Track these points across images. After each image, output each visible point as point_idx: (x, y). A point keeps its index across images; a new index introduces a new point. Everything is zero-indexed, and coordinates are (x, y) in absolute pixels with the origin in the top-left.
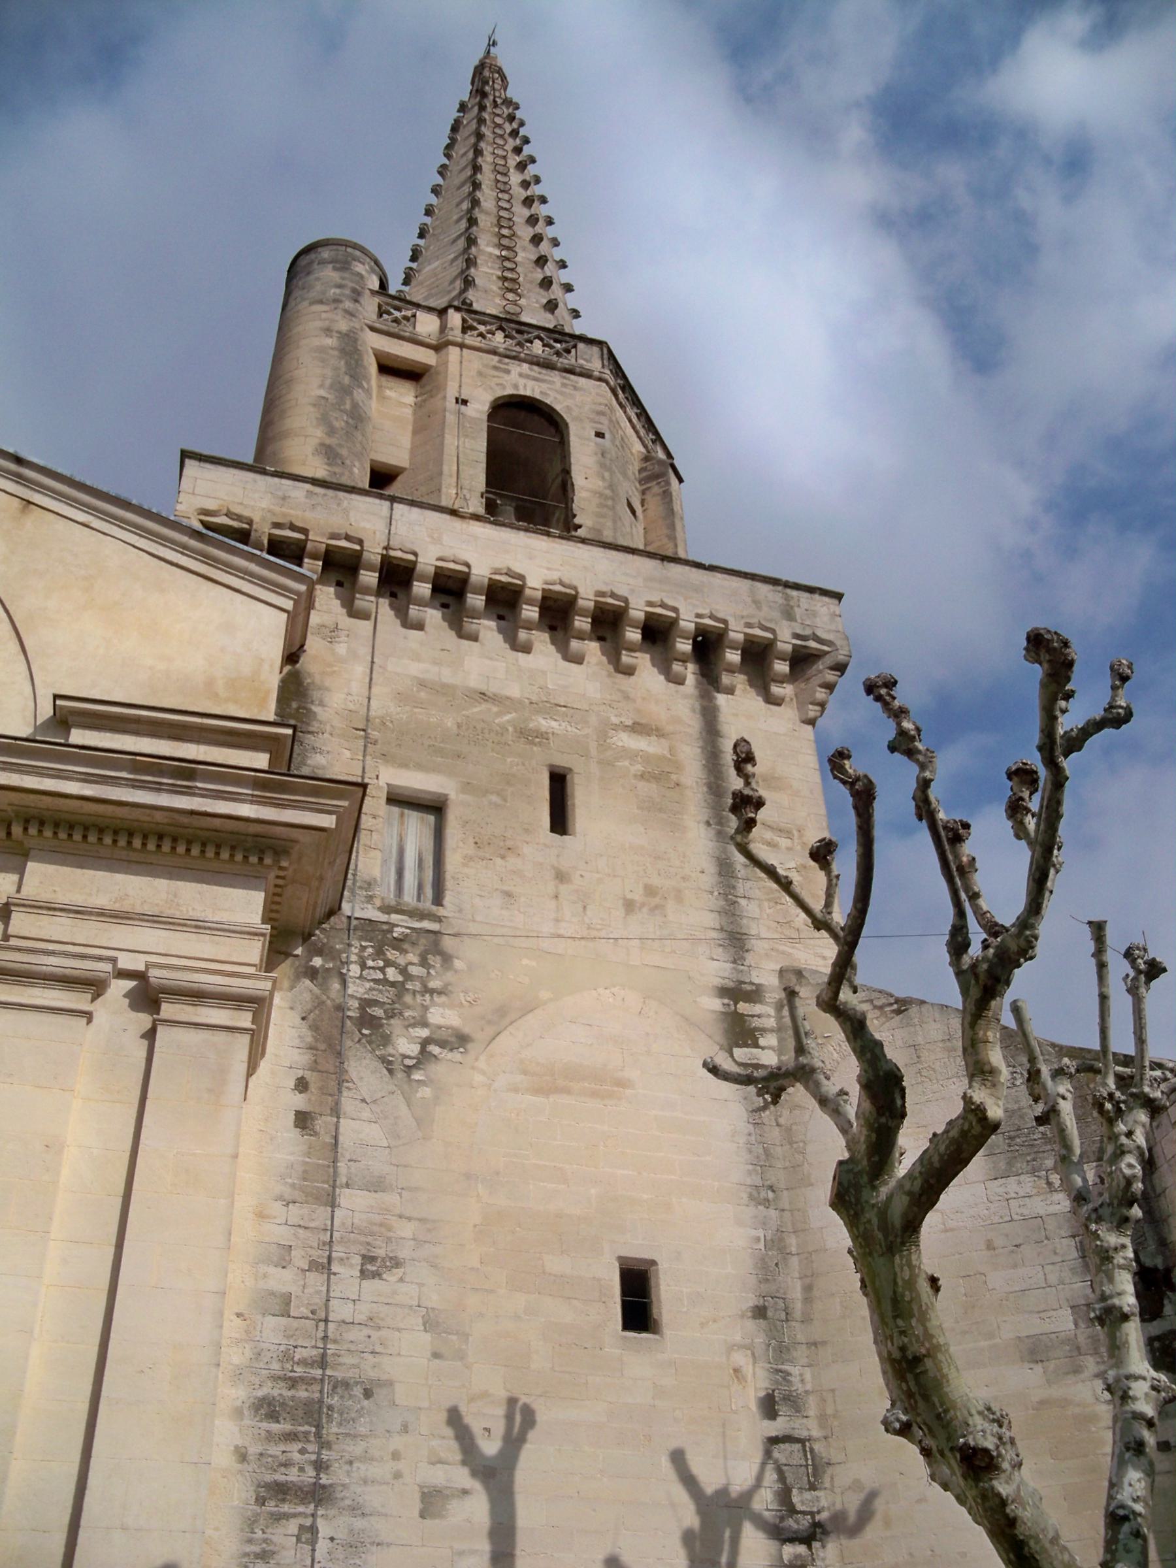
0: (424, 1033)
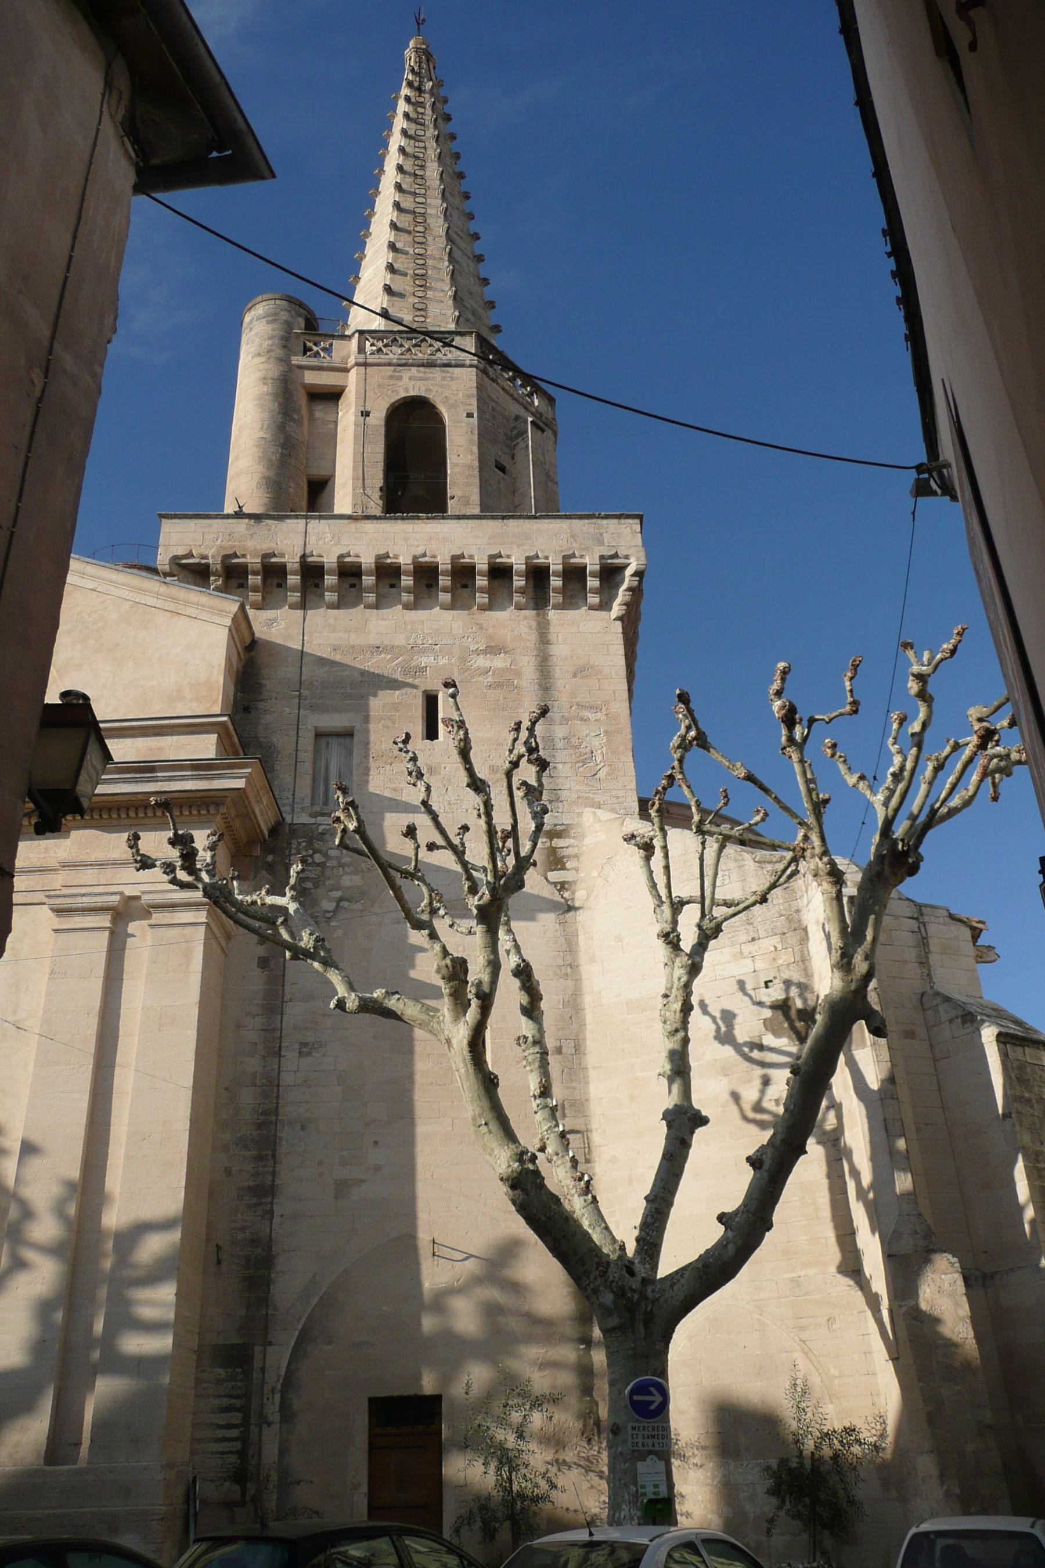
0: (338, 894)
